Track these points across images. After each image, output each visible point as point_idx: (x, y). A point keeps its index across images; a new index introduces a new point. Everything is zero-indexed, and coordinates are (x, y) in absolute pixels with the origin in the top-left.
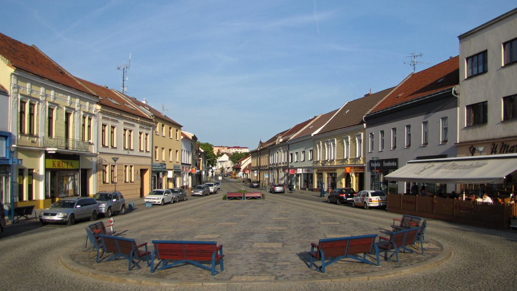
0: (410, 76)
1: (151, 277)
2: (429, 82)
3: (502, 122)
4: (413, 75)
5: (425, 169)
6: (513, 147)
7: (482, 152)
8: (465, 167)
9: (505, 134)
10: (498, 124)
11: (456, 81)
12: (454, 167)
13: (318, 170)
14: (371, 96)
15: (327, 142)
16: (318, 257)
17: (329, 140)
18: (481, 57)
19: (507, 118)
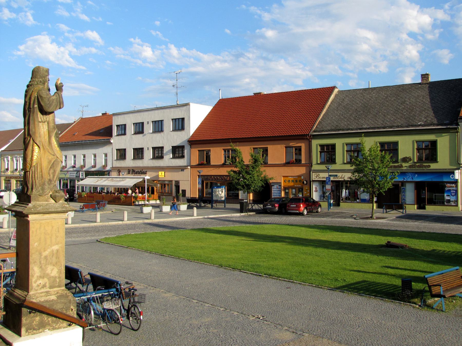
0: (80, 119)
1: (166, 182)
2: (95, 130)
3: (133, 160)
4: (81, 119)
5: (98, 181)
6: (137, 172)
7: (124, 174)
8: (117, 181)
9: (134, 165)
10: (131, 160)
11: (111, 135)
12: (113, 181)
13: (6, 178)
14: (164, 215)
15: (17, 157)
16: (427, 76)
17: (18, 156)
18: (123, 126)
19: (134, 158)
